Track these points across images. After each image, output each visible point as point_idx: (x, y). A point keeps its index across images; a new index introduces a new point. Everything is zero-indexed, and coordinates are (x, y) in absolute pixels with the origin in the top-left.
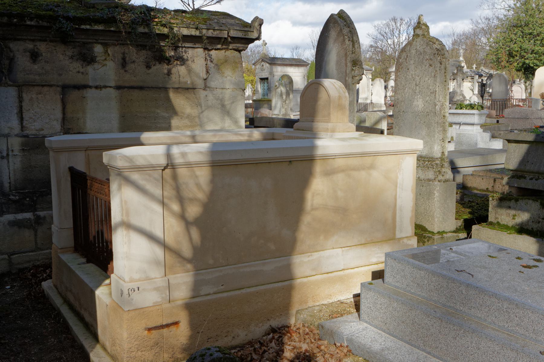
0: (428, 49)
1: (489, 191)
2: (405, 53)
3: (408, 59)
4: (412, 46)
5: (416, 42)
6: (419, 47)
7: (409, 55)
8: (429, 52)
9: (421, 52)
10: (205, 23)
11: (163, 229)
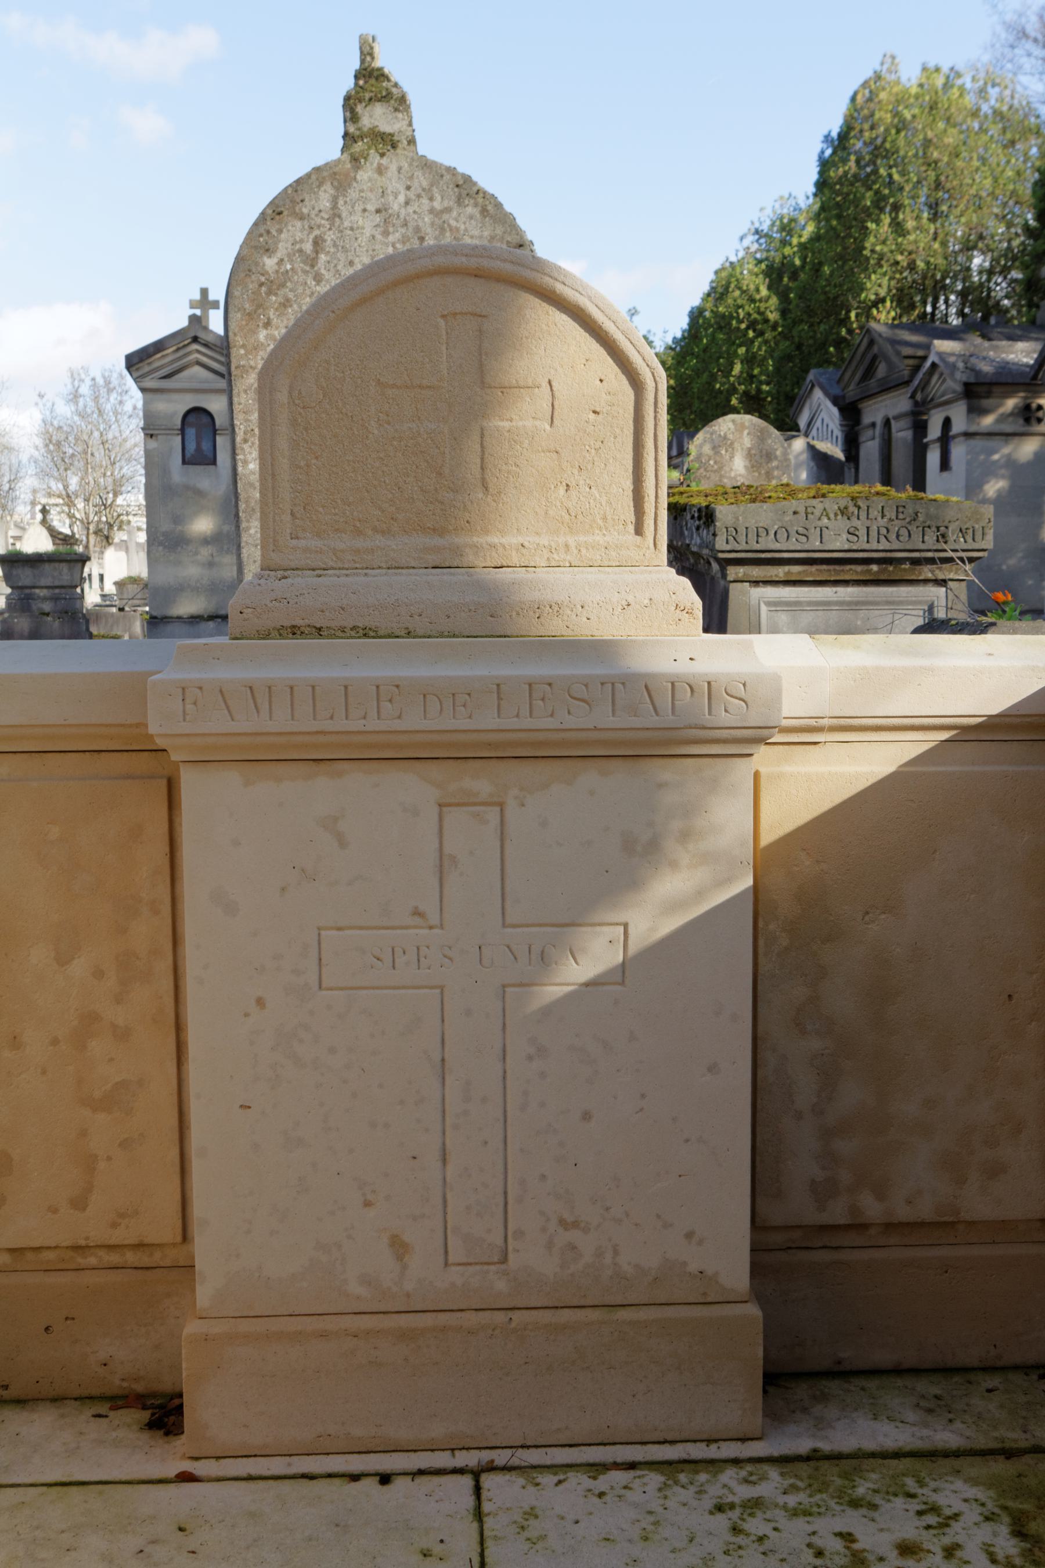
0: (471, 217)
1: (1000, 1454)
2: (299, 224)
3: (323, 257)
4: (353, 194)
5: (380, 170)
6: (402, 198)
7: (330, 237)
8: (476, 233)
9: (417, 229)
10: (27, 591)
11: (22, 754)
